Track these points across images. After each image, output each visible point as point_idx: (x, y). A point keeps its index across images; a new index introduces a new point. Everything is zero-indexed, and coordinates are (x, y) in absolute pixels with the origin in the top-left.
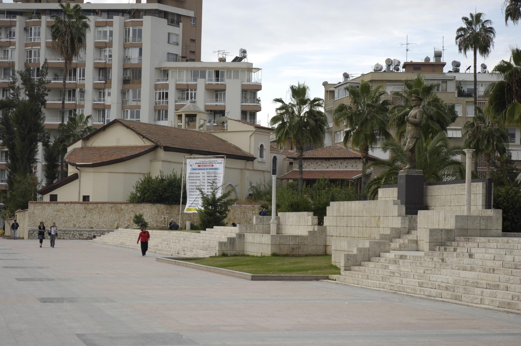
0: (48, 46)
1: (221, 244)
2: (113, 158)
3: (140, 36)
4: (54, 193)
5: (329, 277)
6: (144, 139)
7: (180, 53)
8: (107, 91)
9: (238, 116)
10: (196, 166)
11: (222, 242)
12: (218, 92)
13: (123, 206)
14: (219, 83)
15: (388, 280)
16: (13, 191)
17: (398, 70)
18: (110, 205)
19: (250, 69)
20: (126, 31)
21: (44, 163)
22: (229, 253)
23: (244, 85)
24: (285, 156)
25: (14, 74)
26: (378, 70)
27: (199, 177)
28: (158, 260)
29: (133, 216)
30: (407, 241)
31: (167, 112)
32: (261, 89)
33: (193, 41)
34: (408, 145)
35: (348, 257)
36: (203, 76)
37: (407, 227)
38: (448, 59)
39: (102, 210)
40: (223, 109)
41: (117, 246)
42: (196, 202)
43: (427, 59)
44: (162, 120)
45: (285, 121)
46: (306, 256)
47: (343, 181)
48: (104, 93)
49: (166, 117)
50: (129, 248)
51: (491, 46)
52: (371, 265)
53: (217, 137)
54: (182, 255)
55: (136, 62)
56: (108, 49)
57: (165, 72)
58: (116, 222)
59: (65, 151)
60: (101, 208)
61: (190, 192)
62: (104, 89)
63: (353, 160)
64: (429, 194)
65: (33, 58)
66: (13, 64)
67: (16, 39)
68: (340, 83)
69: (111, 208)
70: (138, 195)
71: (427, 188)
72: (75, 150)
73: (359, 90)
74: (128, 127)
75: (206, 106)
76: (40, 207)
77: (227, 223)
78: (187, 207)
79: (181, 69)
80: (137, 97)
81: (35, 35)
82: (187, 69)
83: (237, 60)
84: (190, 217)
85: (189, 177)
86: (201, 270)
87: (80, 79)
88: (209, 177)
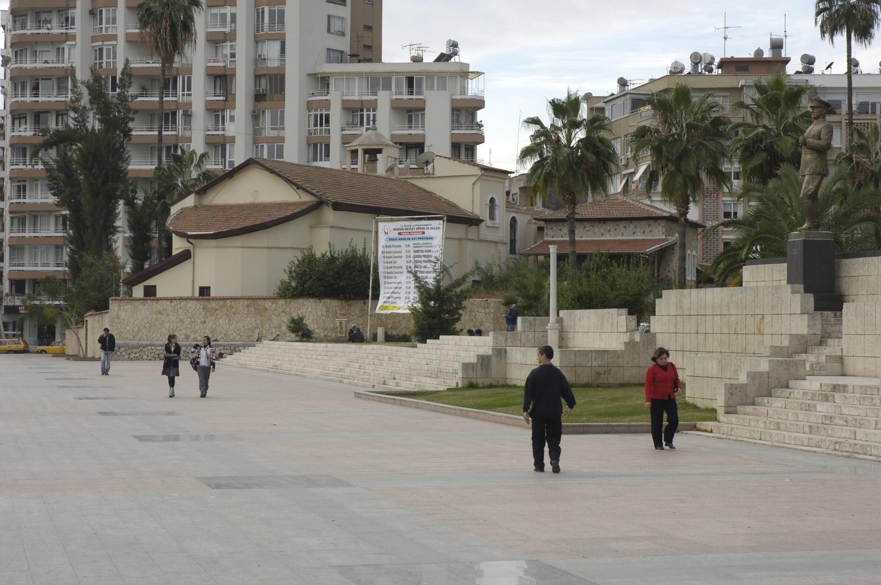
0: (130, 40)
1: (466, 366)
2: (248, 223)
3: (282, 20)
4: (150, 282)
5: (698, 426)
6: (300, 191)
7: (347, 49)
8: (228, 114)
9: (447, 151)
10: (395, 234)
11: (467, 364)
12: (411, 112)
13: (268, 304)
14: (414, 97)
15: (823, 432)
16: (82, 280)
17: (711, 71)
18: (246, 302)
19: (465, 73)
20: (258, 13)
21: (127, 235)
22: (480, 381)
23: (456, 100)
24: (529, 217)
25: (75, 86)
26: (676, 71)
27: (400, 252)
28: (358, 395)
29: (285, 319)
30: (823, 358)
31: (327, 147)
32: (483, 107)
33: (368, 28)
34: (806, 188)
35: (732, 390)
36: (387, 87)
37: (819, 332)
38: (794, 54)
39: (234, 310)
40: (421, 141)
41: (268, 371)
42: (396, 295)
43: (759, 52)
44: (321, 160)
45: (545, 154)
46: (622, 385)
47: (629, 256)
48: (223, 117)
49: (327, 155)
50: (289, 374)
51: (876, 26)
52: (777, 403)
53: (417, 187)
54: (392, 386)
55: (276, 65)
56: (228, 44)
57: (323, 81)
58: (257, 331)
59: (166, 211)
60: (231, 307)
61: (385, 277)
62: (223, 111)
63: (644, 222)
64: (844, 274)
65: (105, 60)
66: (72, 71)
67: (77, 29)
68: (613, 94)
69: (248, 306)
70: (293, 284)
71: (840, 263)
72: (183, 210)
73: (670, 97)
74: (272, 171)
75: (392, 136)
76: (128, 307)
77: (462, 330)
78: (380, 303)
79: (350, 76)
80: (279, 122)
81: (108, 22)
82: (360, 75)
83: (443, 58)
84: (381, 320)
85: (383, 252)
86: (450, 414)
87: (183, 95)
88: (417, 251)
